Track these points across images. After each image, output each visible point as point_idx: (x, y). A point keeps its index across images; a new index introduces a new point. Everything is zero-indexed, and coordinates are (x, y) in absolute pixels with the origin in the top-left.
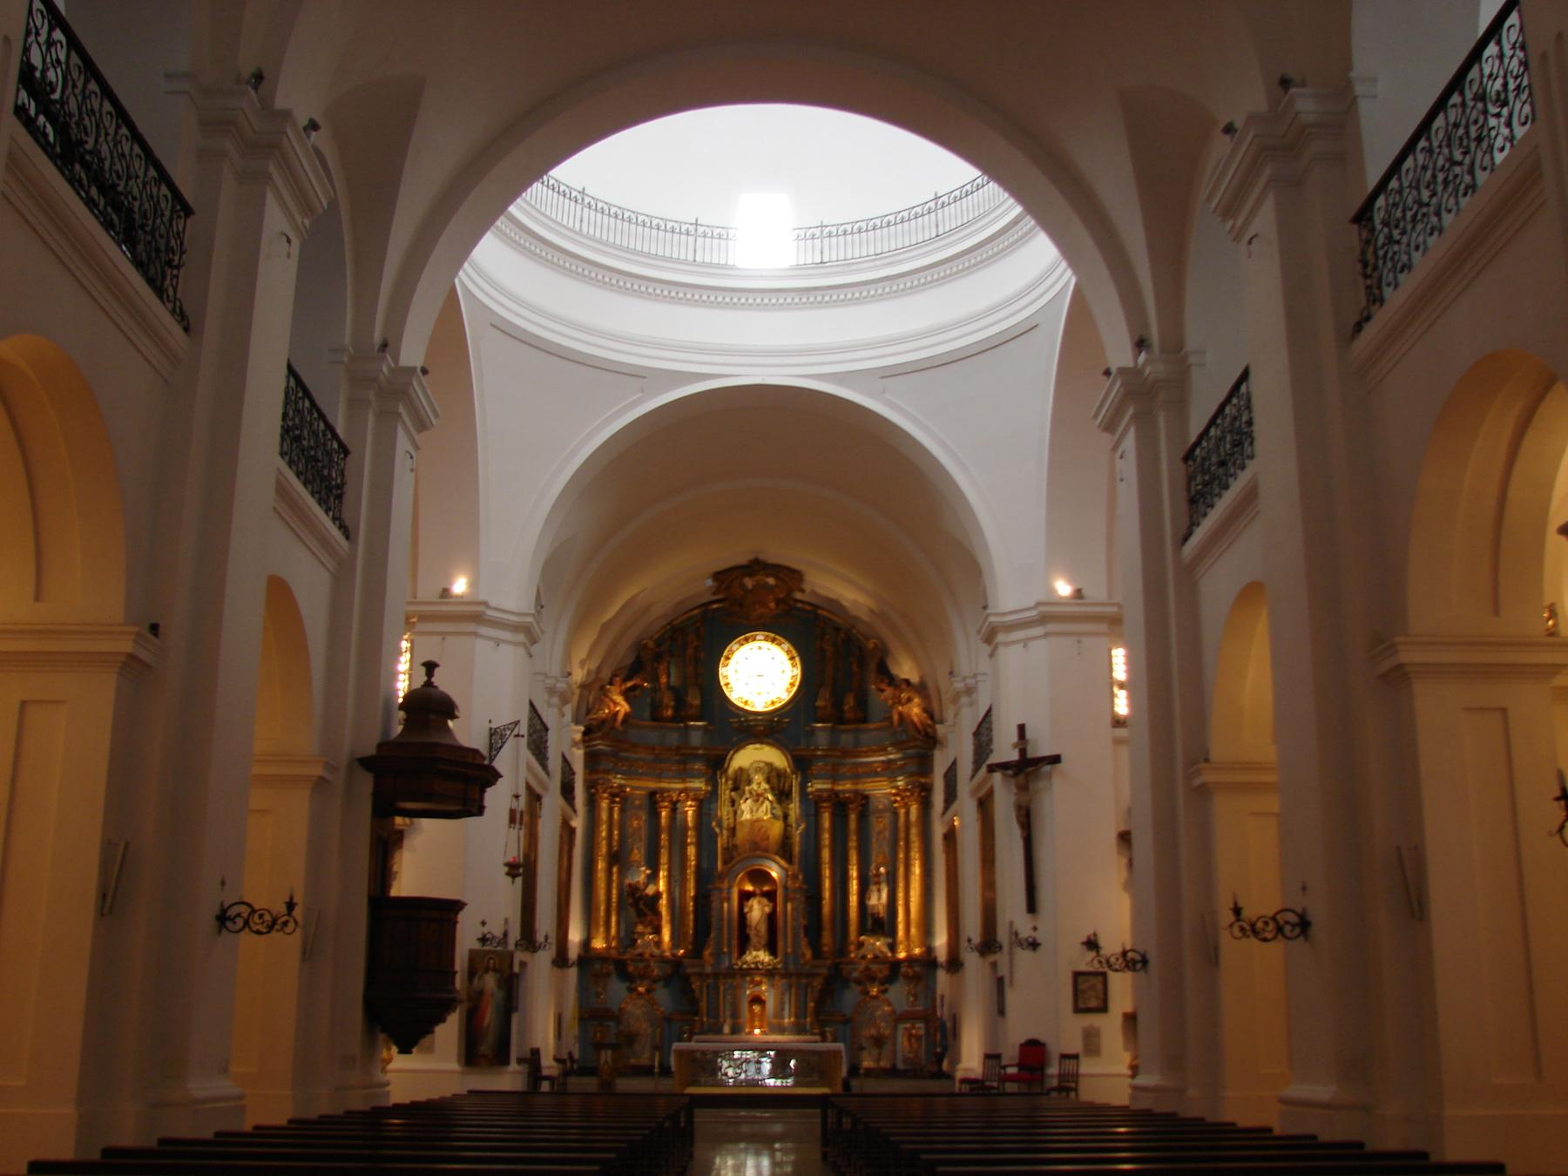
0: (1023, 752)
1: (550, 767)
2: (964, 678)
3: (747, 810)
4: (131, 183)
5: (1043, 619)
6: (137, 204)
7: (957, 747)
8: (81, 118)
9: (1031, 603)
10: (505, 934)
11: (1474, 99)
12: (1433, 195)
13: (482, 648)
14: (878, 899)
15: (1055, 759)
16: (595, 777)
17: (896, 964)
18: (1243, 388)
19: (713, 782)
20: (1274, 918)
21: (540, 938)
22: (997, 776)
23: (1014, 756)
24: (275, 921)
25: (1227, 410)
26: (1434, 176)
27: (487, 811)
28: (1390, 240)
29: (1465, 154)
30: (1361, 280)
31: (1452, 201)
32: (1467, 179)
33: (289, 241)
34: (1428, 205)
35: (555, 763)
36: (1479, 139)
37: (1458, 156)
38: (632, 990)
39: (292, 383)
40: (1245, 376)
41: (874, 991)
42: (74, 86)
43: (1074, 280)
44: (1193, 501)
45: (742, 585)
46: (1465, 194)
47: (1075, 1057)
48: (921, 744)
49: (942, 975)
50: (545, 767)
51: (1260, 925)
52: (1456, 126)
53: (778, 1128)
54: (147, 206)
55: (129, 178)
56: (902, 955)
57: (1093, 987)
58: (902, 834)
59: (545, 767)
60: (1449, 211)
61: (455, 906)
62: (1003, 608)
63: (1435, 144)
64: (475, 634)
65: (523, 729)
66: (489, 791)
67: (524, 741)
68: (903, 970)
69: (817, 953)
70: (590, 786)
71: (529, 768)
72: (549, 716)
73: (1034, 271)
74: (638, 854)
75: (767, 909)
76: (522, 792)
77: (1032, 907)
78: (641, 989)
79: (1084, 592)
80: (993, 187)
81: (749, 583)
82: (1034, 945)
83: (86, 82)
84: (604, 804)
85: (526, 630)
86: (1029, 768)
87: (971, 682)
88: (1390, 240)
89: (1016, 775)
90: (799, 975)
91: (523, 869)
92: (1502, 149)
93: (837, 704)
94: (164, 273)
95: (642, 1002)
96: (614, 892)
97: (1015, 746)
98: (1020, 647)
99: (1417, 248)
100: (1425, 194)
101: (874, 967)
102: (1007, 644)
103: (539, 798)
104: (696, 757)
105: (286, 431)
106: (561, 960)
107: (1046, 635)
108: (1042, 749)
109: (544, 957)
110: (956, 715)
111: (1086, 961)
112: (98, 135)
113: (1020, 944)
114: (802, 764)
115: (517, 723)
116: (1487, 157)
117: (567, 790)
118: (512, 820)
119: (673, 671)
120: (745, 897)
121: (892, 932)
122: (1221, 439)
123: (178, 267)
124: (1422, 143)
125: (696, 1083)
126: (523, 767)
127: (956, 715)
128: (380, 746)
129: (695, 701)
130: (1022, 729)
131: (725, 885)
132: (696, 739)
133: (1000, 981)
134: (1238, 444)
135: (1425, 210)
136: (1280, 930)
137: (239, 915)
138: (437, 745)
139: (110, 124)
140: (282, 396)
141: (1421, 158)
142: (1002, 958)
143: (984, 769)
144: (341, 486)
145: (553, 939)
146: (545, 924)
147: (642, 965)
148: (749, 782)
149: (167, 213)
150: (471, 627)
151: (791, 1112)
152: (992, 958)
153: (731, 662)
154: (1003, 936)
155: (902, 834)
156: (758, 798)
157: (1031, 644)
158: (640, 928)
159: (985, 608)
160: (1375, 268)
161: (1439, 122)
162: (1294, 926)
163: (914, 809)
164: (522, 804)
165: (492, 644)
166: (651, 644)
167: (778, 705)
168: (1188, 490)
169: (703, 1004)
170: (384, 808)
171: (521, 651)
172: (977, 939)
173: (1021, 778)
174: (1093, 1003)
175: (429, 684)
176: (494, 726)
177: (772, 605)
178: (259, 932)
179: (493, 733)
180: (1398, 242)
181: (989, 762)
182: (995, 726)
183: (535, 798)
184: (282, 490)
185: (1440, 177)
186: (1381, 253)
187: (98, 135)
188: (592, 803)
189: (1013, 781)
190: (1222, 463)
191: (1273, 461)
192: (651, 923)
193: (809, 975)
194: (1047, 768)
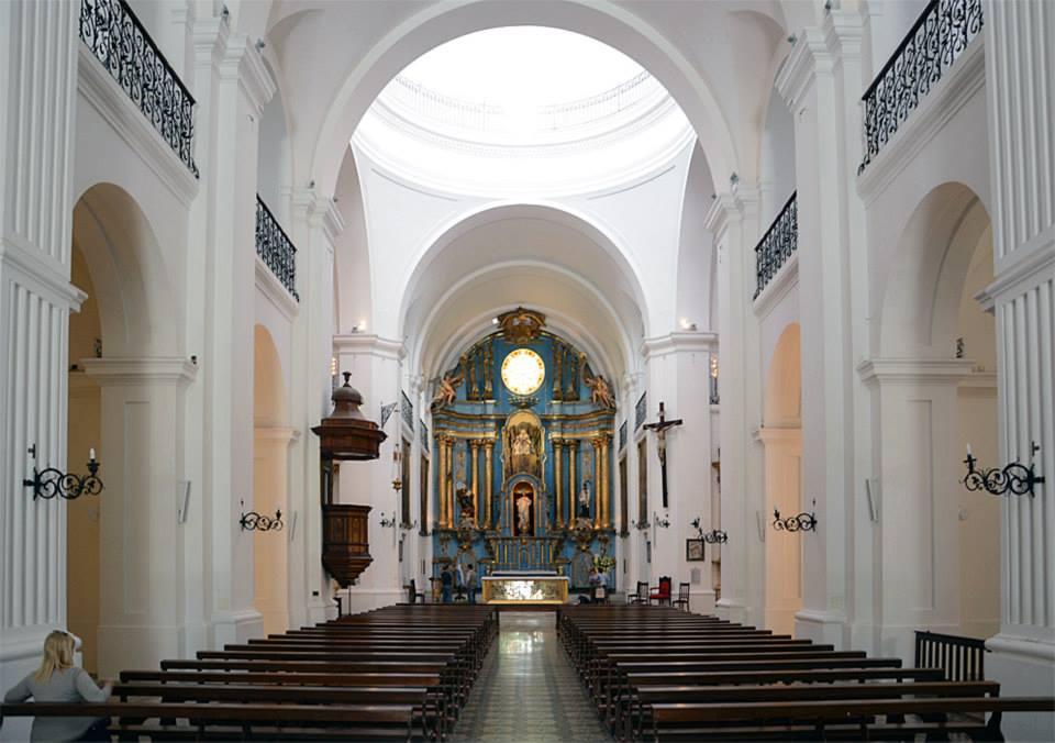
0: (662, 418)
2: (631, 376)
3: (518, 450)
4: (156, 83)
5: (675, 342)
6: (161, 97)
7: (626, 413)
8: (122, 41)
9: (668, 333)
10: (394, 520)
11: (944, 15)
12: (914, 80)
14: (583, 498)
15: (680, 422)
17: (595, 533)
18: (792, 206)
19: (498, 432)
20: (797, 519)
21: (412, 522)
22: (648, 431)
25: (782, 219)
26: (915, 68)
28: (885, 110)
29: (935, 53)
30: (866, 136)
31: (925, 84)
32: (936, 69)
33: (252, 120)
34: (910, 87)
35: (416, 425)
36: (945, 43)
37: (931, 55)
39: (261, 209)
40: (794, 196)
41: (584, 548)
42: (116, 19)
43: (696, 137)
44: (760, 275)
45: (512, 322)
46: (933, 80)
47: (688, 585)
48: (607, 411)
49: (618, 538)
50: (411, 427)
51: (992, 477)
52: (931, 34)
53: (534, 622)
54: (167, 98)
55: (155, 80)
56: (597, 527)
57: (697, 547)
59: (411, 427)
60: (923, 92)
61: (368, 509)
63: (917, 46)
64: (372, 354)
65: (399, 407)
66: (382, 445)
67: (400, 414)
69: (555, 527)
70: (436, 437)
71: (403, 428)
72: (413, 401)
73: (673, 133)
75: (529, 504)
76: (400, 443)
77: (665, 505)
79: (698, 327)
80: (652, 80)
82: (667, 524)
83: (123, 16)
84: (443, 448)
86: (663, 425)
87: (635, 377)
88: (885, 109)
90: (545, 539)
91: (403, 485)
92: (959, 50)
93: (563, 389)
94: (181, 141)
98: (661, 359)
99: (901, 116)
100: (909, 80)
101: (583, 535)
103: (409, 445)
104: (490, 420)
105: (259, 238)
106: (424, 532)
107: (676, 351)
109: (416, 531)
110: (627, 396)
111: (694, 534)
112: (134, 52)
113: (659, 524)
114: (546, 422)
115: (396, 404)
116: (949, 54)
118: (395, 458)
120: (517, 496)
122: (778, 237)
123: (189, 137)
124: (909, 46)
125: (493, 598)
126: (400, 427)
127: (627, 396)
128: (322, 421)
130: (662, 405)
132: (490, 410)
133: (649, 543)
134: (787, 240)
135: (907, 91)
136: (800, 525)
138: (353, 420)
139: (140, 43)
140: (255, 216)
141: (907, 55)
142: (650, 531)
143: (641, 427)
144: (292, 271)
145: (419, 522)
146: (415, 515)
147: (465, 534)
148: (519, 434)
149: (180, 102)
150: (370, 350)
151: (543, 614)
152: (644, 531)
153: (508, 366)
154: (650, 519)
156: (523, 442)
157: (668, 356)
158: (464, 514)
159: (643, 336)
160: (875, 129)
161: (921, 31)
162: (808, 523)
163: (605, 449)
164: (400, 450)
165: (380, 359)
167: (541, 361)
168: (758, 268)
169: (497, 554)
170: (329, 459)
172: (637, 522)
173: (661, 432)
174: (697, 556)
175: (346, 385)
176: (384, 405)
178: (263, 530)
180: (890, 112)
181: (644, 423)
182: (647, 403)
183: (407, 445)
184: (259, 273)
185: (919, 68)
186: (879, 119)
187: (134, 52)
188: (437, 446)
189: (656, 434)
190: (778, 252)
191: (799, 111)
192: (469, 511)
193: (551, 539)
194: (675, 427)
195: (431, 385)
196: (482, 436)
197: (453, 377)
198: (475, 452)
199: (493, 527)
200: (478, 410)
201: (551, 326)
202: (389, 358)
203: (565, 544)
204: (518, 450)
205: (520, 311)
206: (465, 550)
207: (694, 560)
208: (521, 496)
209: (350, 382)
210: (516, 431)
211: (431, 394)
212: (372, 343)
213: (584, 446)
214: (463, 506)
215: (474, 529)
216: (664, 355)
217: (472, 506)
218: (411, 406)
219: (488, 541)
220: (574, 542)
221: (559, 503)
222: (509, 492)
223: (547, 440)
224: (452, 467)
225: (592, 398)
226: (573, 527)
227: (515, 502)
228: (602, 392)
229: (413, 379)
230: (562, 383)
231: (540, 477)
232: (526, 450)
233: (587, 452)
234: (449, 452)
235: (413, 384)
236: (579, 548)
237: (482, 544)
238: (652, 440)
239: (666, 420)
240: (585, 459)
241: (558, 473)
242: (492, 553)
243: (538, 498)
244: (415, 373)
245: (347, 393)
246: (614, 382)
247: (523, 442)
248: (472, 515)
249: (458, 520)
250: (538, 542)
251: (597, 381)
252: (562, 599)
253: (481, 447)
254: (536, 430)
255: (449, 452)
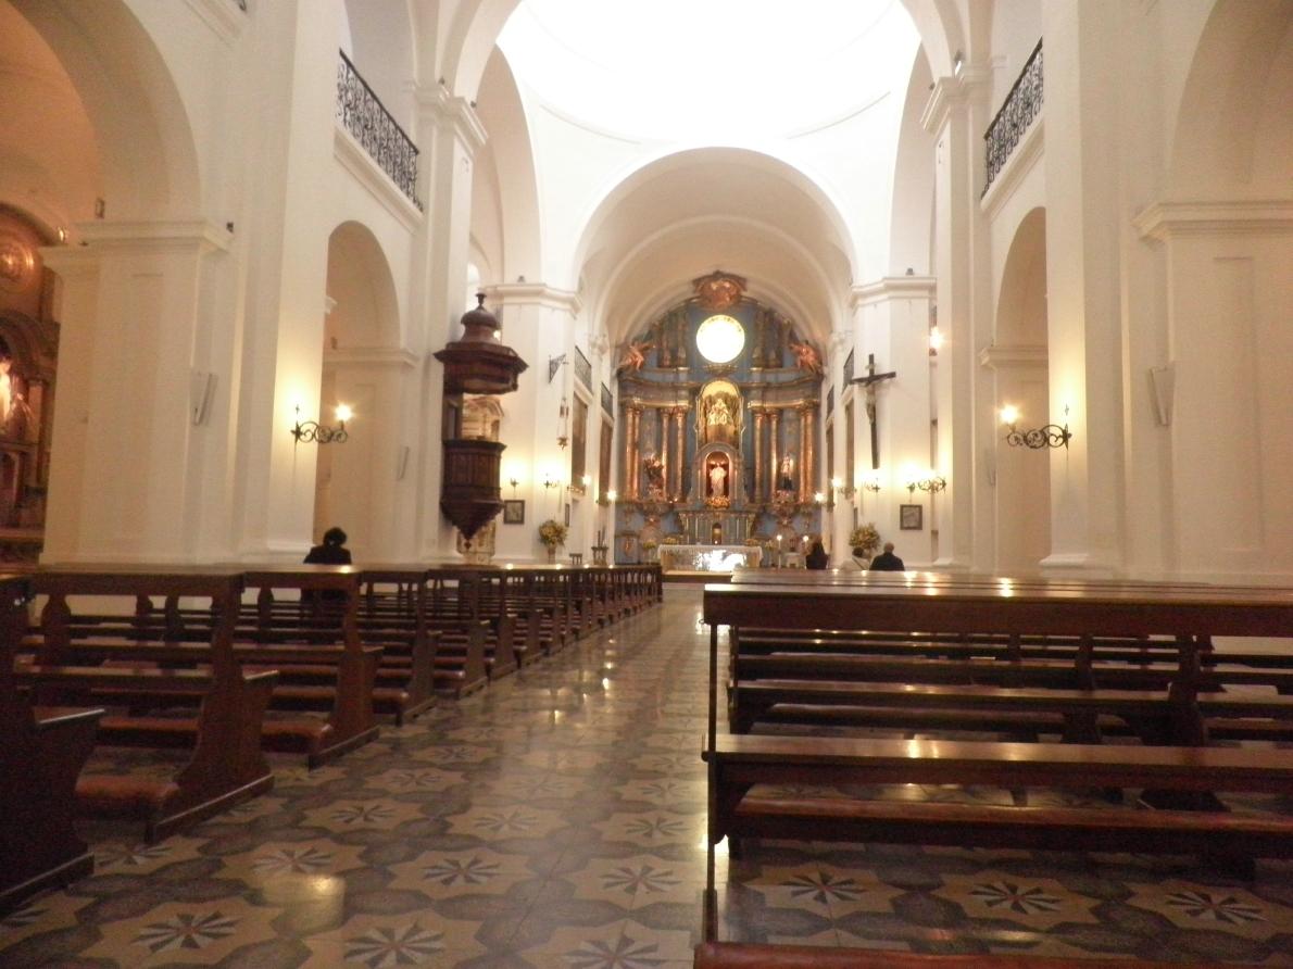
0: (872, 371)
1: (593, 388)
2: (840, 333)
3: (713, 419)
7: (836, 376)
9: (880, 279)
13: (543, 313)
15: (892, 375)
16: (624, 399)
18: (1036, 62)
19: (692, 402)
23: (866, 374)
24: (332, 434)
27: (519, 388)
38: (646, 520)
40: (1039, 46)
41: (785, 522)
44: (990, 164)
45: (710, 287)
48: (814, 378)
50: (589, 388)
51: (1031, 436)
57: (913, 514)
58: (803, 432)
59: (589, 388)
62: (861, 283)
64: (539, 304)
68: (802, 510)
69: (752, 500)
70: (623, 406)
71: (576, 385)
72: (593, 360)
74: (650, 444)
76: (571, 404)
78: (652, 520)
81: (714, 286)
84: (630, 416)
85: (572, 302)
86: (873, 380)
89: (867, 385)
90: (741, 512)
95: (652, 528)
96: (636, 465)
97: (867, 368)
101: (785, 508)
102: (863, 306)
103: (586, 407)
108: (883, 367)
114: (745, 391)
117: (606, 405)
119: (443, 99)
121: (797, 489)
125: (673, 569)
129: (683, 355)
130: (871, 358)
131: (699, 460)
132: (683, 377)
137: (308, 430)
138: (482, 344)
147: (651, 507)
148: (715, 403)
155: (803, 432)
156: (719, 412)
158: (651, 486)
159: (850, 284)
163: (810, 418)
165: (550, 310)
166: (657, 323)
170: (453, 389)
171: (568, 315)
173: (870, 386)
174: (912, 524)
175: (480, 308)
177: (728, 299)
179: (551, 363)
188: (623, 415)
189: (865, 389)
194: (886, 381)
195: (619, 350)
196: (672, 404)
197: (644, 341)
198: (665, 421)
199: (683, 500)
200: (670, 377)
201: (727, 270)
202: (558, 309)
203: (764, 519)
204: (713, 419)
205: (717, 275)
206: (651, 524)
207: (909, 528)
208: (713, 467)
209: (484, 305)
210: (712, 401)
211: (618, 359)
212: (539, 293)
213: (790, 415)
214: (650, 477)
215: (662, 499)
216: (875, 304)
217: (660, 476)
218: (590, 366)
219: (677, 514)
220: (775, 517)
221: (758, 475)
222: (702, 462)
223: (745, 409)
224: (639, 437)
225: (796, 365)
226: (771, 503)
227: (708, 474)
228: (810, 358)
229: (593, 339)
230: (763, 350)
231: (738, 448)
232: (723, 420)
233: (790, 421)
234: (637, 420)
235: (593, 345)
236: (780, 523)
237: (671, 518)
238: (860, 396)
239: (876, 373)
240: (788, 429)
241: (758, 444)
242: (682, 527)
243: (734, 469)
244: (596, 333)
245: (479, 314)
246: (821, 348)
247: (719, 412)
248: (660, 487)
249: (643, 492)
250: (733, 515)
251: (801, 345)
252: (944, 790)
253: (672, 416)
254: (734, 399)
255: (637, 420)
